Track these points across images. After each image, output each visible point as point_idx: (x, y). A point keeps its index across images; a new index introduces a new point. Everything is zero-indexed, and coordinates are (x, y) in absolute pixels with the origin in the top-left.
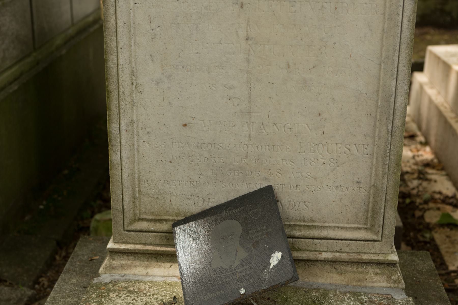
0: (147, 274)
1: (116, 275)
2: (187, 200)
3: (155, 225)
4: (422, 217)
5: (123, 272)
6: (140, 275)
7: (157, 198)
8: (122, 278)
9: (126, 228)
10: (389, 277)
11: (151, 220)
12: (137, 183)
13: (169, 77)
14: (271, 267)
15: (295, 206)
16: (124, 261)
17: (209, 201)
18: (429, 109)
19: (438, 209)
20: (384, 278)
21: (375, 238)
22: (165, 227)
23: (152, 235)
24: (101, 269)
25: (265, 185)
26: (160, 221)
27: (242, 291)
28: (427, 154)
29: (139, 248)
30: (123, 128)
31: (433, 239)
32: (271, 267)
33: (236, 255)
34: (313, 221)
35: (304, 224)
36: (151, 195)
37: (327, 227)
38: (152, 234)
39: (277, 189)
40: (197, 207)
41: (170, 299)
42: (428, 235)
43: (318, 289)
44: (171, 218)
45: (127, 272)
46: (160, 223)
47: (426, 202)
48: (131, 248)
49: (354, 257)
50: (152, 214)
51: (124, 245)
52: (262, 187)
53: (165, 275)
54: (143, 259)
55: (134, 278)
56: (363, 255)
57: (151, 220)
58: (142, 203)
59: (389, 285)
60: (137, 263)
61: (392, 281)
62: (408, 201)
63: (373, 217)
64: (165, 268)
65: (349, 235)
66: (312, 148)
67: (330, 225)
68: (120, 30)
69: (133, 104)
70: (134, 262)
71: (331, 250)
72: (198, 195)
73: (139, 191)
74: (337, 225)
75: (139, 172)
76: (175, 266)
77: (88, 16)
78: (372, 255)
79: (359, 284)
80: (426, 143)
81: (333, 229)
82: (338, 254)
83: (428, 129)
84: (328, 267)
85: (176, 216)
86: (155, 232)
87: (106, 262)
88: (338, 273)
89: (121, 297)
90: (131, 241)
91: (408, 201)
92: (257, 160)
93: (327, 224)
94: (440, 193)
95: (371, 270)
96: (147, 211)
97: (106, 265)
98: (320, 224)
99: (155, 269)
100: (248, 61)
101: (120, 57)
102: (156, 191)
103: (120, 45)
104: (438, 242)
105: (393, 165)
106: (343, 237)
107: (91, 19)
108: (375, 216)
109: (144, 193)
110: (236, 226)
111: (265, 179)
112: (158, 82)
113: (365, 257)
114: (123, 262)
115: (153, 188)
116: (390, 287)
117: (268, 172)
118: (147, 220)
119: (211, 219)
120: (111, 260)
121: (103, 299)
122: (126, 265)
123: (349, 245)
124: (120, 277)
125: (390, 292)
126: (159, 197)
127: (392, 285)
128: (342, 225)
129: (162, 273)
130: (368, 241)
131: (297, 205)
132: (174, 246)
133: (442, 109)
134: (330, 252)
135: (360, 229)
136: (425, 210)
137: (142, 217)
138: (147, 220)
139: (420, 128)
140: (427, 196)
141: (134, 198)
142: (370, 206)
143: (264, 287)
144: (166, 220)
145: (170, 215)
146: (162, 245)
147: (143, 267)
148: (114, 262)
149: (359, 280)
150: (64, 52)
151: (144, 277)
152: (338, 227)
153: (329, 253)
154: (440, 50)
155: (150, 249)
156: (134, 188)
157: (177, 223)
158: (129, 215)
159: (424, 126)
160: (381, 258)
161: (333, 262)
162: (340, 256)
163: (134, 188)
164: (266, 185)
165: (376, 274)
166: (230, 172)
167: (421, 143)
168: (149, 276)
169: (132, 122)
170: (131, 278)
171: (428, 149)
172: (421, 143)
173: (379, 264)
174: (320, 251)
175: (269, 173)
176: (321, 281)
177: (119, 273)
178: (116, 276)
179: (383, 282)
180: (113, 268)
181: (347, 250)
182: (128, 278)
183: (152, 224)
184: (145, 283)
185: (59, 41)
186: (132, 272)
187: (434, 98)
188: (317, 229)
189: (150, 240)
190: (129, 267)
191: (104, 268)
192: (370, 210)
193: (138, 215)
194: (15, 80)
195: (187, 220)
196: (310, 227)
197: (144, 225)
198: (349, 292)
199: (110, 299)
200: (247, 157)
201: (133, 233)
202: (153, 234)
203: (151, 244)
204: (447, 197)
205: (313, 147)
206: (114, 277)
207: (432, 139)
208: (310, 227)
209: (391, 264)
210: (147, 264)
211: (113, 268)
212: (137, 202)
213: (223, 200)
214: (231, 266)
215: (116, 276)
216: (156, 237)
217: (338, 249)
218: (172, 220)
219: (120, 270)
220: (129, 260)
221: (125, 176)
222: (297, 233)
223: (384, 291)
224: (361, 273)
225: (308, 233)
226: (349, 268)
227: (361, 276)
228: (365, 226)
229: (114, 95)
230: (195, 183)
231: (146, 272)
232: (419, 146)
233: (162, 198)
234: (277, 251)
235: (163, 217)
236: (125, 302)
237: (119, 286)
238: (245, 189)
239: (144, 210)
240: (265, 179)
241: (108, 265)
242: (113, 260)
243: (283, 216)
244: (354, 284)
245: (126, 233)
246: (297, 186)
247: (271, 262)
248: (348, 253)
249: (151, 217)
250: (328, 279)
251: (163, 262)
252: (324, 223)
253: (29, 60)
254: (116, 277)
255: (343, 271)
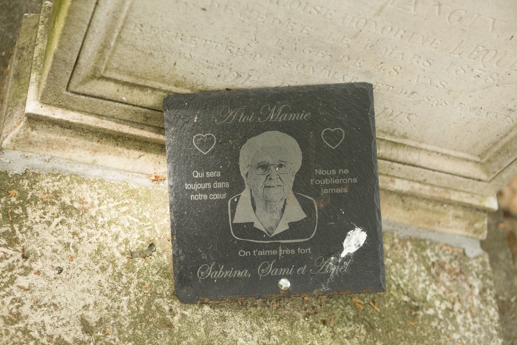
0: (94, 162)
1: (35, 155)
2: (206, 69)
3: (130, 91)
5: (49, 153)
6: (80, 163)
7: (151, 54)
8: (49, 166)
9: (72, 88)
10: (471, 224)
12: (120, 25)
14: (343, 255)
15: (390, 115)
16: (54, 135)
17: (247, 79)
20: (465, 224)
21: (484, 177)
23: (119, 107)
25: (361, 79)
26: (143, 88)
29: (89, 123)
32: (343, 255)
33: (283, 211)
34: (404, 137)
35: (389, 139)
36: (139, 48)
37: (421, 149)
38: (120, 105)
39: (387, 113)
40: (221, 82)
41: (140, 242)
44: (165, 87)
45: (58, 154)
46: (141, 90)
48: (74, 121)
49: (439, 193)
50: (130, 74)
51: (60, 110)
52: (353, 82)
53: (127, 169)
54: (91, 136)
55: (69, 168)
56: (452, 192)
58: (116, 55)
59: (466, 234)
61: (473, 229)
64: (129, 158)
65: (448, 166)
66: (476, 53)
67: (429, 147)
70: (73, 140)
71: (411, 178)
72: (232, 66)
73: (119, 37)
74: (439, 150)
75: (131, 9)
78: (464, 195)
79: (427, 226)
81: (429, 153)
82: (417, 186)
85: (176, 86)
86: (126, 104)
88: (404, 208)
89: (49, 223)
90: (75, 107)
92: (369, 45)
93: (423, 146)
96: (121, 68)
97: (17, 136)
98: (413, 144)
99: (110, 156)
102: (153, 44)
106: (440, 168)
108: (501, 152)
109: (127, 43)
114: (52, 136)
115: (149, 39)
116: (467, 236)
117: (378, 65)
120: (29, 130)
121: (16, 227)
122: (57, 141)
123: (440, 178)
124: (42, 163)
126: (156, 54)
127: (470, 234)
128: (445, 151)
130: (469, 178)
131: (395, 115)
134: (408, 180)
135: (468, 160)
137: (108, 74)
138: (116, 81)
141: (105, 46)
142: (504, 141)
144: (154, 89)
145: (164, 82)
146: (133, 122)
147: (88, 149)
148: (34, 133)
149: (430, 222)
151: (87, 167)
152: (438, 153)
153: (406, 182)
155: (110, 128)
162: (421, 189)
164: (362, 81)
165: (456, 217)
166: (311, 49)
168: (98, 167)
170: (63, 167)
174: (394, 177)
175: (379, 67)
177: (42, 153)
179: (461, 228)
180: (31, 143)
181: (434, 182)
182: (57, 165)
183: (126, 89)
184: (90, 183)
186: (67, 155)
188: (405, 148)
190: (63, 146)
191: (12, 141)
192: (500, 145)
193: (103, 71)
197: (108, 89)
198: (411, 239)
199: (30, 228)
200: (355, 36)
201: (83, 97)
202: (124, 105)
203: (111, 118)
205: (478, 52)
206: (30, 162)
210: (98, 147)
211: (31, 143)
212: (108, 53)
214: (272, 228)
216: (126, 110)
217: (422, 179)
218: (165, 91)
219: (44, 148)
220: (64, 134)
224: (438, 212)
225: (389, 152)
227: (434, 217)
228: (478, 159)
230: (235, 50)
231: (93, 158)
233: (161, 56)
234: (359, 226)
235: (149, 83)
236: (60, 242)
237: (41, 188)
239: (115, 65)
241: (21, 137)
242: (33, 129)
244: (421, 225)
245: (70, 94)
246: (413, 93)
247: (345, 244)
248: (432, 185)
249: (126, 79)
251: (128, 148)
252: (421, 142)
255: (413, 205)
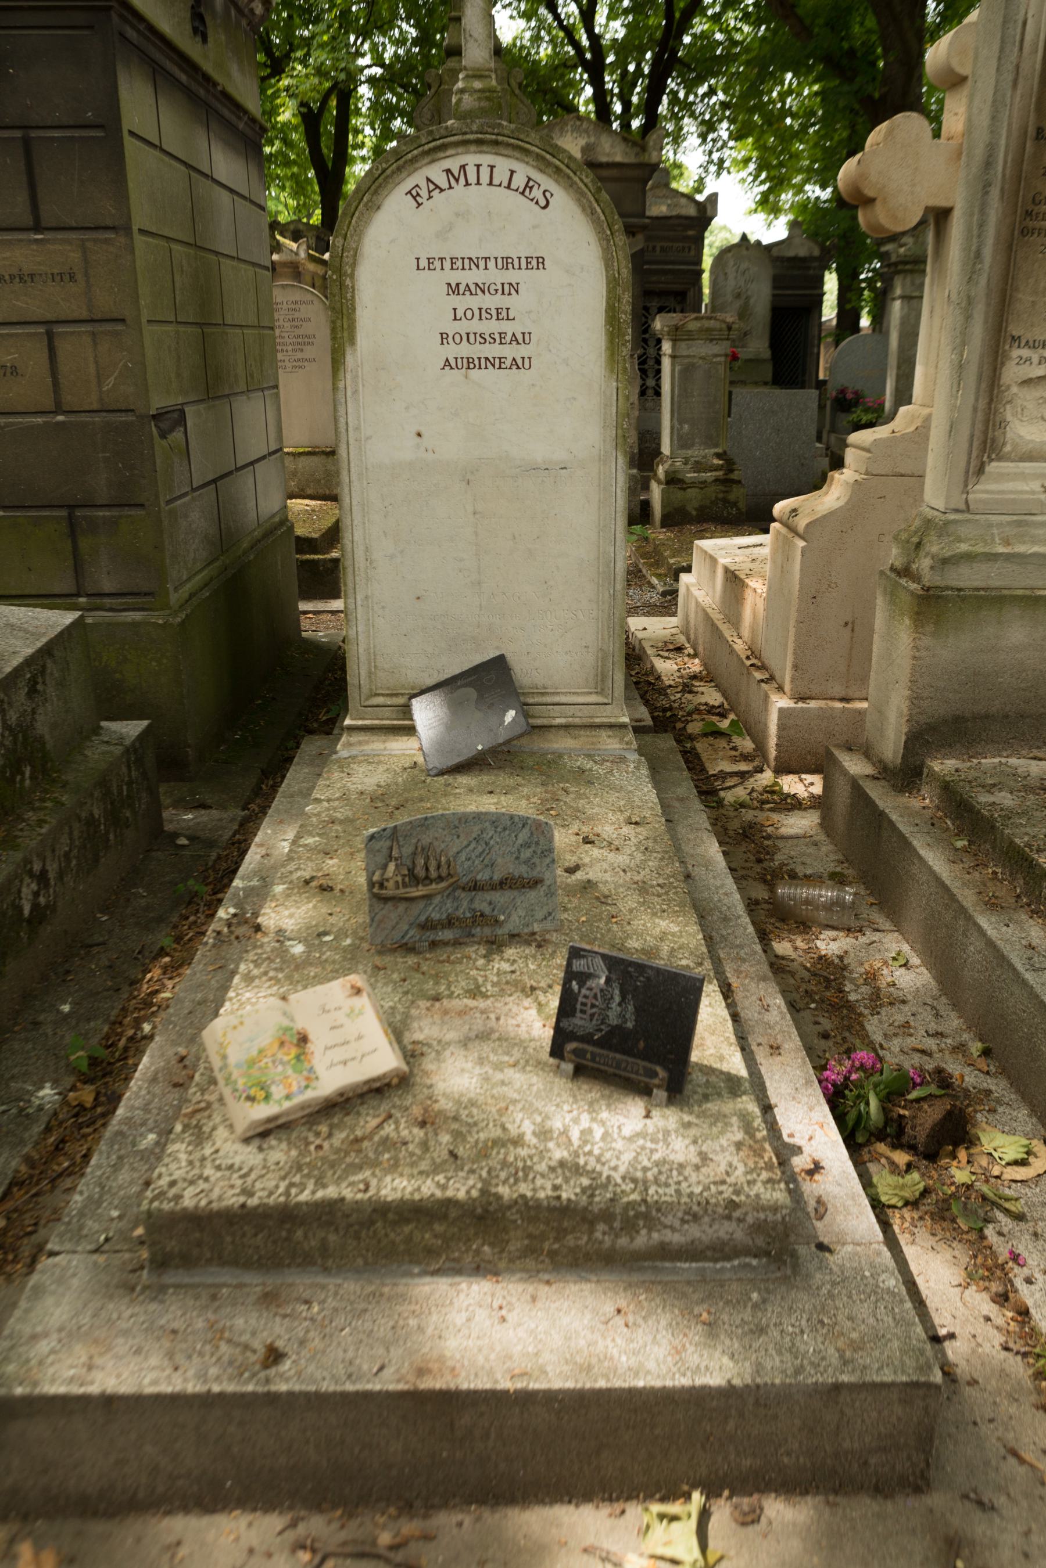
4: (685, 728)
11: (387, 695)
13: (402, 552)
18: (696, 613)
19: (703, 720)
21: (606, 701)
22: (401, 700)
24: (339, 747)
25: (498, 653)
26: (396, 695)
27: (480, 748)
28: (695, 666)
30: (359, 602)
31: (694, 748)
39: (511, 659)
42: (688, 745)
43: (553, 753)
47: (690, 714)
57: (387, 695)
60: (375, 738)
62: (669, 714)
63: (602, 681)
68: (354, 508)
69: (368, 579)
76: (413, 739)
77: (273, 516)
80: (695, 655)
83: (696, 639)
84: (562, 732)
87: (344, 739)
91: (669, 714)
94: (706, 704)
95: (604, 733)
100: (476, 534)
101: (356, 534)
103: (355, 522)
104: (699, 750)
105: (617, 628)
107: (277, 519)
110: (472, 693)
111: (497, 648)
112: (392, 557)
113: (597, 720)
118: (383, 695)
119: (446, 689)
125: (622, 753)
129: (401, 747)
132: (412, 719)
133: (709, 610)
136: (688, 722)
139: (688, 640)
140: (691, 707)
141: (370, 673)
143: (501, 741)
150: (252, 557)
154: (707, 544)
156: (369, 663)
157: (415, 696)
158: (365, 690)
159: (692, 636)
160: (613, 720)
161: (566, 727)
163: (369, 663)
167: (689, 655)
169: (367, 597)
171: (697, 661)
172: (689, 655)
173: (611, 726)
176: (555, 746)
178: (355, 751)
185: (245, 545)
187: (700, 600)
189: (387, 715)
190: (367, 742)
194: (206, 585)
195: (422, 692)
196: (543, 694)
197: (380, 700)
204: (713, 707)
207: (701, 649)
208: (543, 694)
209: (623, 726)
213: (457, 671)
215: (355, 751)
221: (361, 651)
222: (531, 701)
223: (617, 752)
226: (582, 732)
227: (595, 740)
229: (350, 570)
232: (686, 659)
238: (478, 659)
240: (497, 648)
243: (517, 684)
250: (562, 743)
253: (216, 564)
254: (355, 753)
